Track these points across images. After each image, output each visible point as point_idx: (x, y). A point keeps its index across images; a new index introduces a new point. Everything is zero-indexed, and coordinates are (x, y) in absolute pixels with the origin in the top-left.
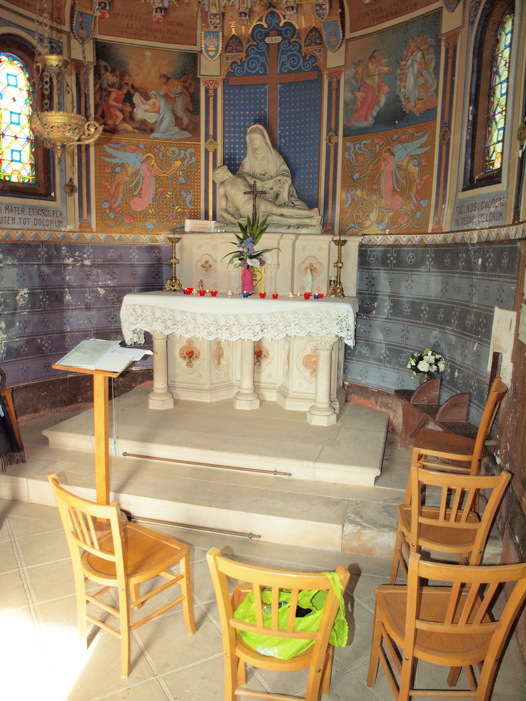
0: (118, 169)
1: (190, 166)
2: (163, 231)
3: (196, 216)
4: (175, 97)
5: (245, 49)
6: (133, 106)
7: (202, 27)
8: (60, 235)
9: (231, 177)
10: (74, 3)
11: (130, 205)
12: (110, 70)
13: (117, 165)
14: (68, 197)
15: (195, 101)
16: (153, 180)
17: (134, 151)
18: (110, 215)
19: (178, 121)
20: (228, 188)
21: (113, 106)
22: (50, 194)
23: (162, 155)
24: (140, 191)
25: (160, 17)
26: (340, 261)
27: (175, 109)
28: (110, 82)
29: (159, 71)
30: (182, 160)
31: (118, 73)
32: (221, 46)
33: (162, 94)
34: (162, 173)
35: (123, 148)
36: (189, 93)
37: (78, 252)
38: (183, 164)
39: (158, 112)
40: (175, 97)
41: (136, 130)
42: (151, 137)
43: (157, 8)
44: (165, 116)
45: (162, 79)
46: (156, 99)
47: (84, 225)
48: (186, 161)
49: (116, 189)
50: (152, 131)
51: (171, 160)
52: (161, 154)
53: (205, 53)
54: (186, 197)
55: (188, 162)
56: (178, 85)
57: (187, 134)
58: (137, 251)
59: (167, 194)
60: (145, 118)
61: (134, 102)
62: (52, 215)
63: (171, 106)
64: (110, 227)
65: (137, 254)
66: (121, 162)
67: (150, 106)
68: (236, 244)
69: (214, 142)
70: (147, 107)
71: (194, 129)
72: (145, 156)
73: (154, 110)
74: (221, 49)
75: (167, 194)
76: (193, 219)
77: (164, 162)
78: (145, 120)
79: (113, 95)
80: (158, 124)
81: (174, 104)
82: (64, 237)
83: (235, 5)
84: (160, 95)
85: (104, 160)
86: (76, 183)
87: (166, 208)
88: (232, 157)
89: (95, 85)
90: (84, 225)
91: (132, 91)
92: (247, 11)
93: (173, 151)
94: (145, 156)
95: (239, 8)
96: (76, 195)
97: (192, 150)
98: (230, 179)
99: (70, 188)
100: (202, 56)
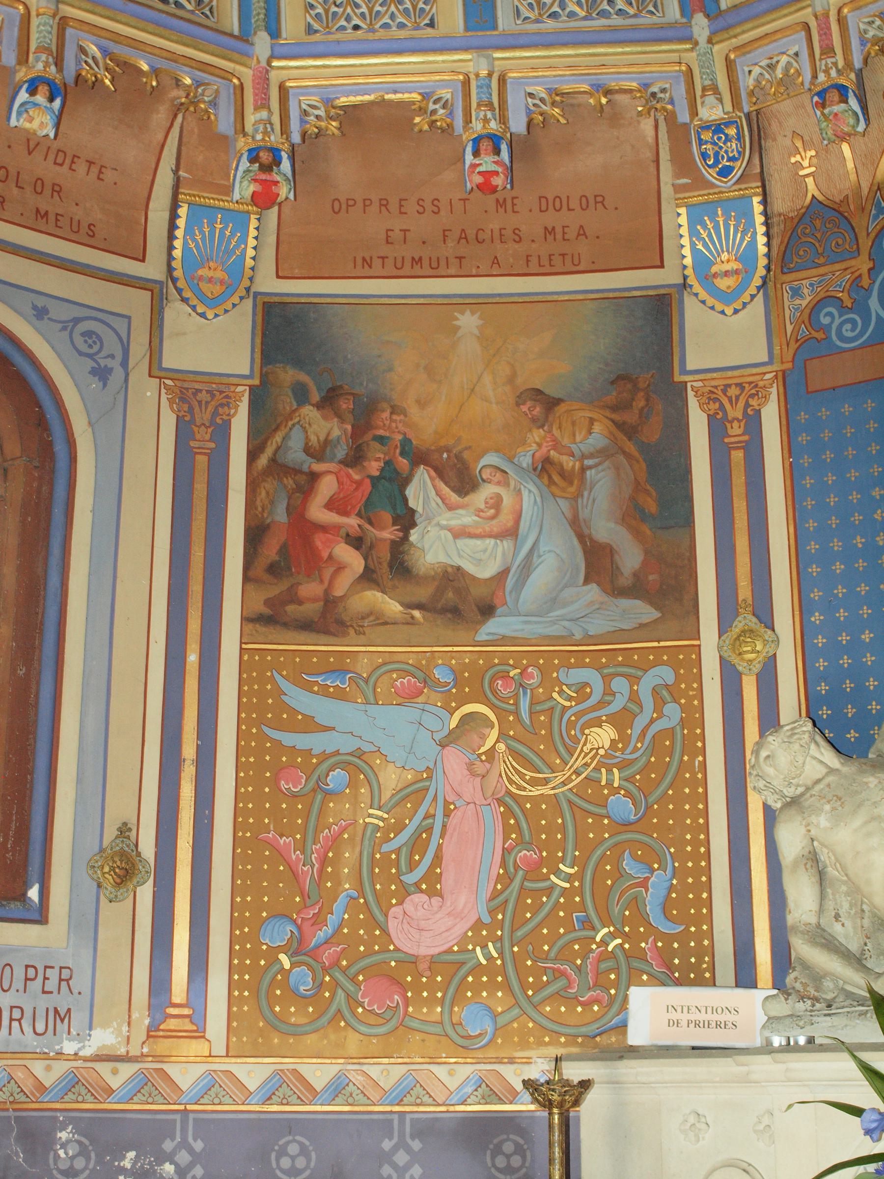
1: (655, 746)
4: (583, 470)
5: (865, 243)
6: (407, 520)
7: (677, 189)
8: (50, 1074)
9: (831, 771)
11: (385, 932)
17: (410, 696)
18: (292, 980)
19: (598, 562)
20: (823, 821)
21: (324, 528)
22: (22, 897)
23: (532, 704)
25: (494, 168)
27: (583, 514)
28: (313, 439)
29: (511, 380)
30: (621, 721)
31: (345, 405)
32: (762, 249)
33: (526, 461)
34: (534, 782)
35: (366, 690)
37: (131, 1154)
38: (624, 738)
39: (512, 532)
41: (417, 614)
43: (477, 141)
44: (543, 548)
45: (524, 408)
46: (505, 483)
47: (172, 1024)
48: (640, 722)
49: (324, 861)
50: (487, 610)
51: (571, 725)
52: (524, 705)
53: (697, 288)
54: (644, 883)
56: (592, 421)
57: (642, 611)
58: (416, 1145)
59: (557, 872)
60: (458, 561)
61: (412, 504)
62: (18, 984)
63: (564, 504)
64: (297, 1032)
65: (415, 1157)
66: (347, 745)
67: (478, 512)
68: (856, 1111)
69: (761, 629)
70: (465, 518)
71: (667, 587)
73: (495, 526)
74: (762, 262)
75: (557, 872)
76: (678, 983)
77: (541, 738)
78: (459, 568)
79: (327, 487)
80: (510, 582)
81: (579, 494)
82: (73, 1082)
85: (277, 743)
86: (147, 847)
87: (553, 939)
89: (252, 456)
90: (172, 1024)
91: (403, 463)
92: (849, 80)
93: (582, 689)
95: (815, 76)
96: (146, 893)
97: (665, 674)
98: (830, 779)
99: (121, 867)
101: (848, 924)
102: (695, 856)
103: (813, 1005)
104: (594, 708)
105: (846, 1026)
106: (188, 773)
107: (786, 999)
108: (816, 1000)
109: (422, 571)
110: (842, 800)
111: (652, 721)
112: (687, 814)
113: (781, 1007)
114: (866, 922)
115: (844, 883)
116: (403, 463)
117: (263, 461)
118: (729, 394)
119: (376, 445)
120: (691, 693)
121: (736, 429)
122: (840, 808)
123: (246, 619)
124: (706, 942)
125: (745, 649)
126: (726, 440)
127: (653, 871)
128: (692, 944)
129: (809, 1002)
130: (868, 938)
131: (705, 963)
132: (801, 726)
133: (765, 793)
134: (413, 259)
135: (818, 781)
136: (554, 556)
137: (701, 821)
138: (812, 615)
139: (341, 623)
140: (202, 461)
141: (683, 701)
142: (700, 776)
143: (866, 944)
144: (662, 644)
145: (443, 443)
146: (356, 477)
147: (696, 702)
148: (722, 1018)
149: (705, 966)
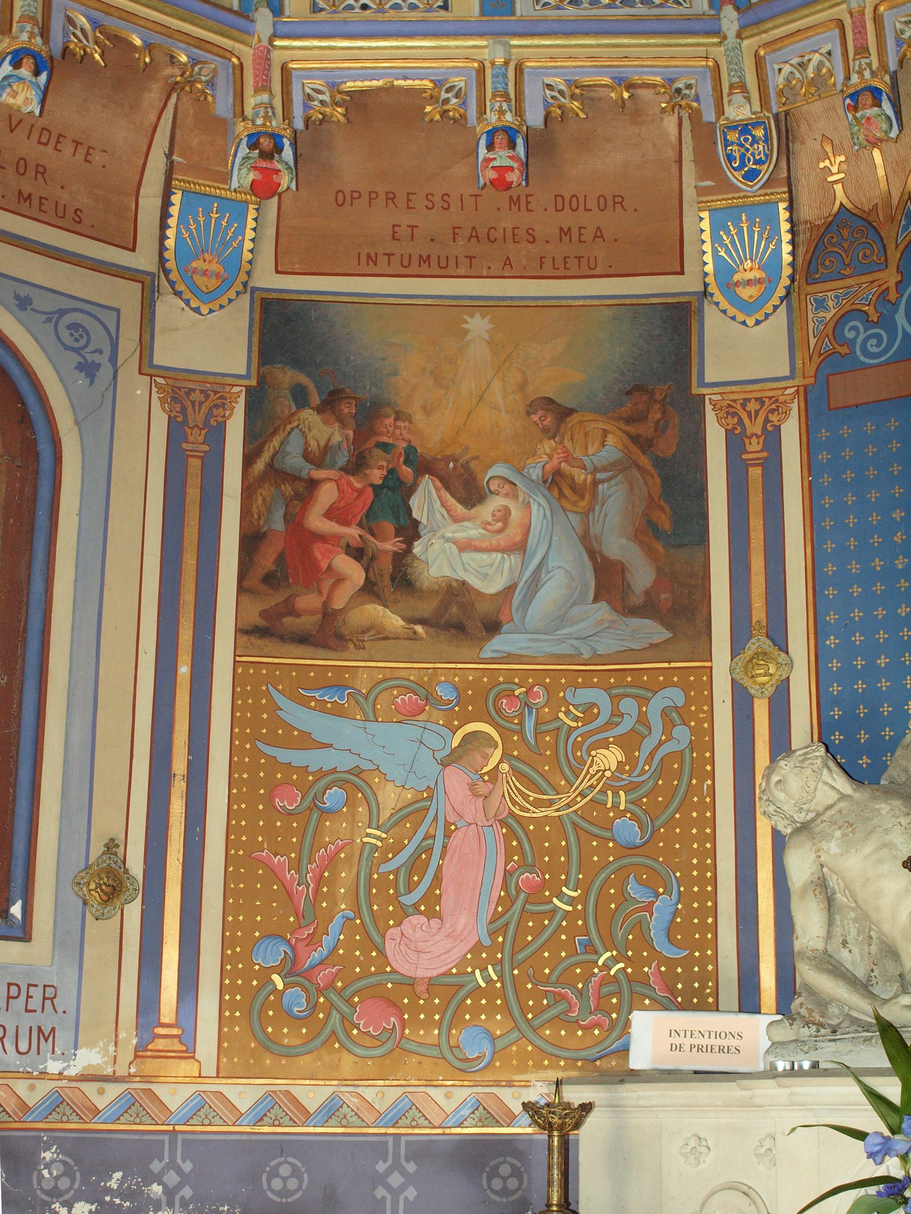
0: (334, 796)
2: (539, 1066)
3: (700, 993)
4: (595, 483)
6: (410, 531)
7: (700, 191)
8: (33, 1094)
9: (843, 797)
10: (172, 163)
11: (382, 953)
12: (316, 400)
13: (330, 777)
14: (89, 918)
15: (680, 488)
16: (494, 836)
17: (410, 714)
19: (608, 580)
20: (834, 847)
21: (323, 538)
23: (537, 724)
24: (431, 889)
26: (789, 177)
27: (595, 529)
28: (313, 444)
29: (522, 387)
30: (630, 743)
31: (347, 409)
32: (787, 258)
33: (536, 473)
34: (537, 804)
36: (660, 463)
37: (118, 1175)
38: (631, 760)
39: (520, 547)
40: (595, 483)
41: (419, 629)
42: (486, 654)
44: (551, 563)
45: (535, 418)
47: (160, 1044)
48: (648, 745)
49: (319, 881)
50: (493, 627)
51: (577, 746)
52: (530, 725)
53: (718, 297)
54: (649, 908)
55: (656, 749)
56: (605, 433)
57: (654, 631)
58: (411, 1167)
59: (560, 895)
61: (415, 514)
63: (574, 519)
64: (290, 1053)
65: (409, 1179)
66: (346, 762)
67: (485, 525)
68: (860, 1135)
69: (775, 652)
70: (471, 531)
71: (680, 608)
72: (460, 734)
73: (501, 540)
74: (787, 271)
76: (681, 1008)
77: (545, 758)
78: (464, 583)
79: (327, 495)
81: (591, 509)
82: (57, 1102)
83: (831, 74)
84: (528, 479)
86: (136, 864)
87: (555, 962)
88: (862, 711)
89: (248, 460)
91: (407, 472)
92: (883, 83)
93: (589, 709)
94: (460, 734)
95: (848, 78)
96: (133, 911)
97: (675, 696)
98: (842, 805)
99: (108, 884)
100: (709, 311)
101: (856, 950)
102: (701, 881)
103: (818, 1031)
104: (600, 730)
105: (851, 1051)
106: (179, 788)
107: (791, 1025)
108: (821, 1025)
109: (426, 585)
110: (853, 827)
111: (660, 744)
112: (694, 838)
113: (786, 1033)
114: (874, 949)
115: (853, 909)
116: (407, 472)
117: (259, 466)
118: (748, 409)
119: (378, 452)
120: (701, 716)
121: (754, 445)
122: (851, 835)
123: (242, 631)
124: (710, 968)
125: (758, 672)
126: (744, 457)
127: (658, 895)
128: (696, 969)
129: (814, 1028)
130: (876, 965)
131: (709, 988)
132: (814, 751)
133: (775, 818)
134: (421, 257)
135: (830, 807)
136: (564, 573)
137: (708, 845)
138: (828, 638)
139: (340, 637)
140: (195, 464)
141: (693, 724)
142: (708, 800)
143: (872, 971)
144: (673, 665)
145: (449, 451)
146: (358, 485)
147: (706, 725)
148: (725, 1043)
149: (708, 991)
